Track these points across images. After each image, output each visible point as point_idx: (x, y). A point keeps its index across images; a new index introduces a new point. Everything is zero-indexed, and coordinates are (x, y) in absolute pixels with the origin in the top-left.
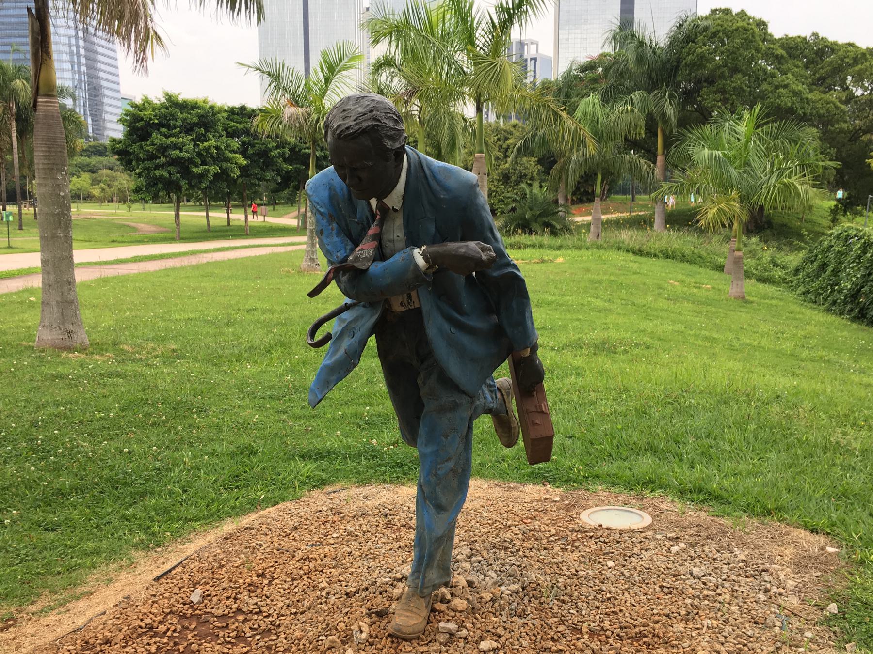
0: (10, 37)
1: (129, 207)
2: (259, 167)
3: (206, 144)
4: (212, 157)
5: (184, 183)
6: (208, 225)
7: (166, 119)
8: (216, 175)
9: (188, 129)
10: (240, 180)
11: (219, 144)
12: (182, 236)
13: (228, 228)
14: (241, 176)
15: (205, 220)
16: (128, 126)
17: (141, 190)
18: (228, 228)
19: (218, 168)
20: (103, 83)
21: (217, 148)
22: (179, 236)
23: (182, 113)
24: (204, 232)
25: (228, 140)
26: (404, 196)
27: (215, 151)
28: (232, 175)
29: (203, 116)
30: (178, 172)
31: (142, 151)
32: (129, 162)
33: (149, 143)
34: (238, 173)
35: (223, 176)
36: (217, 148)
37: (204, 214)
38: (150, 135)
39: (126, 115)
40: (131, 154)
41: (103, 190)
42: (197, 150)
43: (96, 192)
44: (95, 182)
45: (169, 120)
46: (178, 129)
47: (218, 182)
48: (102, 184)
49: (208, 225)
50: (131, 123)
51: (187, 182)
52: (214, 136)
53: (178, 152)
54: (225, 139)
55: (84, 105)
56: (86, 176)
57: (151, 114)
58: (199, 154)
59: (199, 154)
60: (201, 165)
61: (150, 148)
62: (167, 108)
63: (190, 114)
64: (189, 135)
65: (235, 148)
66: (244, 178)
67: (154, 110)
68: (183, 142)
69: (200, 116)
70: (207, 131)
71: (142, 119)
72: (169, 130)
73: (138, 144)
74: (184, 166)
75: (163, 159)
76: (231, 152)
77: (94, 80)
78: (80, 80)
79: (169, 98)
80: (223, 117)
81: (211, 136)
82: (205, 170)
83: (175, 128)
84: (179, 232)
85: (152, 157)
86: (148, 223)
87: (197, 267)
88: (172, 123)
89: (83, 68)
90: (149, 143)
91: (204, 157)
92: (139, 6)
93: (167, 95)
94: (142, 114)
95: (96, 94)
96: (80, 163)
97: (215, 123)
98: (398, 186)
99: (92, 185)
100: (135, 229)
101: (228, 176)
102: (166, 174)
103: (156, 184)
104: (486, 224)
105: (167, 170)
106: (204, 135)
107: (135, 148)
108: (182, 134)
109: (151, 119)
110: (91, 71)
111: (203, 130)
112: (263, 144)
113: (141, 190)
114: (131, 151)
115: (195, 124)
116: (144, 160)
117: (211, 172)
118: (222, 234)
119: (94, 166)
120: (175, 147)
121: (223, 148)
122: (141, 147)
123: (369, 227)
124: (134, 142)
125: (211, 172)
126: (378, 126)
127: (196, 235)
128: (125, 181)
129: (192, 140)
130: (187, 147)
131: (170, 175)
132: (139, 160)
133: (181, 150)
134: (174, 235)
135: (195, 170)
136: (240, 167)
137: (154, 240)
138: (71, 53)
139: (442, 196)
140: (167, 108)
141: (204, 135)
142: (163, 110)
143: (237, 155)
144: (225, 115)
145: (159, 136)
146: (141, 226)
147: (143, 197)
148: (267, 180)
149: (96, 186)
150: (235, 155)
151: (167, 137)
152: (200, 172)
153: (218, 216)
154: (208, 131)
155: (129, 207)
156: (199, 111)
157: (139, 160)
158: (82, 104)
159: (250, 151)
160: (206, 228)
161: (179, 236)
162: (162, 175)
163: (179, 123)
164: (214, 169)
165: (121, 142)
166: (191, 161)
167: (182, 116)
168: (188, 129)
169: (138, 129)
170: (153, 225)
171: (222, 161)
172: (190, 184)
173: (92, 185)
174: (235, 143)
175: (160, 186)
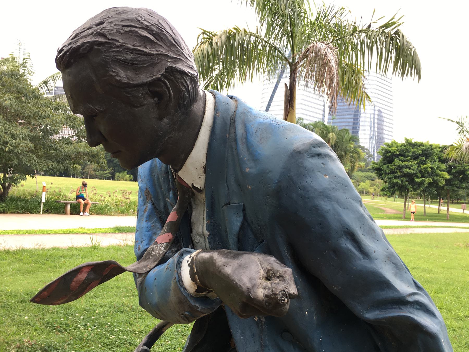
0: (343, 115)
1: (386, 199)
2: (458, 180)
3: (425, 166)
4: (428, 173)
5: (409, 187)
6: (425, 212)
7: (403, 152)
8: (430, 184)
9: (415, 157)
10: (445, 187)
11: (433, 166)
12: (406, 216)
13: (438, 215)
14: (446, 185)
15: (423, 208)
16: (383, 155)
17: (385, 190)
18: (438, 215)
19: (431, 179)
20: (385, 136)
21: (432, 168)
22: (405, 217)
23: (413, 149)
24: (422, 216)
25: (439, 164)
26: (205, 169)
27: (430, 170)
28: (440, 184)
29: (425, 150)
30: (407, 181)
31: (388, 169)
32: (381, 175)
33: (392, 165)
34: (444, 183)
35: (434, 184)
36: (432, 168)
37: (423, 205)
38: (393, 160)
39: (382, 150)
40: (382, 170)
41: (375, 189)
42: (419, 169)
43: (371, 190)
44: (372, 185)
45: (405, 152)
46: (410, 157)
47: (431, 188)
48: (375, 187)
49: (425, 212)
50: (384, 154)
51: (411, 186)
52: (430, 161)
53: (408, 170)
54: (437, 163)
55: (374, 147)
56: (368, 182)
57: (395, 149)
58: (420, 171)
59: (420, 171)
60: (421, 177)
61: (393, 168)
62: (405, 146)
63: (417, 149)
64: (416, 160)
65: (443, 168)
66: (448, 186)
67: (397, 147)
68: (411, 165)
69: (423, 150)
70: (426, 158)
71: (390, 152)
72: (404, 158)
73: (386, 165)
74: (410, 177)
75: (399, 174)
76: (440, 171)
77: (381, 135)
78: (373, 135)
79: (407, 140)
80: (437, 151)
81: (429, 161)
82: (423, 180)
83: (408, 157)
84: (405, 215)
85: (393, 172)
86: (390, 208)
87: (400, 236)
88: (406, 154)
89: (376, 129)
90: (392, 165)
91: (423, 174)
92: (334, 74)
93: (406, 139)
94: (390, 149)
95: (380, 141)
96: (367, 175)
97: (432, 154)
98: (194, 152)
99: (371, 186)
100: (383, 211)
101: (437, 184)
102: (399, 182)
103: (394, 187)
104: (335, 224)
105: (401, 179)
106: (425, 161)
107: (385, 167)
108: (412, 160)
109: (395, 152)
110: (380, 130)
111: (424, 158)
112: (462, 167)
113: (385, 190)
114: (382, 169)
115: (420, 155)
116: (389, 174)
117: (427, 182)
118: (432, 218)
119: (374, 177)
120: (407, 167)
121: (435, 168)
122: (388, 167)
123: (168, 214)
124: (385, 164)
125: (427, 182)
126: (100, 44)
127: (419, 217)
128: (380, 184)
129: (417, 163)
130: (414, 167)
131: (402, 182)
132: (386, 173)
133: (410, 169)
134: (401, 216)
135: (417, 180)
136: (446, 180)
137: (389, 218)
138: (371, 122)
139: (248, 170)
140: (405, 146)
141: (425, 161)
142: (403, 147)
143: (444, 173)
144: (440, 150)
145: (398, 161)
146: (388, 209)
147: (386, 193)
148: (463, 188)
149: (372, 187)
150: (442, 173)
151: (403, 161)
152: (419, 181)
153: (433, 208)
154: (427, 159)
155: (386, 199)
156: (423, 147)
157: (386, 173)
158: (373, 147)
159: (454, 171)
160: (423, 214)
161: (405, 217)
162: (397, 182)
163: (411, 154)
164: (428, 180)
165: (378, 164)
166: (415, 175)
167: (413, 150)
168: (415, 157)
169: (388, 157)
170: (394, 210)
171: (434, 176)
172: (413, 187)
173: (371, 186)
174: (444, 166)
175: (396, 188)
